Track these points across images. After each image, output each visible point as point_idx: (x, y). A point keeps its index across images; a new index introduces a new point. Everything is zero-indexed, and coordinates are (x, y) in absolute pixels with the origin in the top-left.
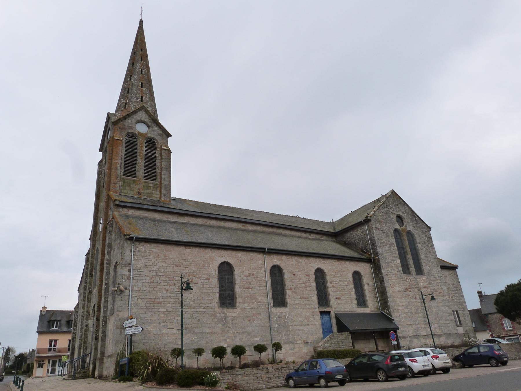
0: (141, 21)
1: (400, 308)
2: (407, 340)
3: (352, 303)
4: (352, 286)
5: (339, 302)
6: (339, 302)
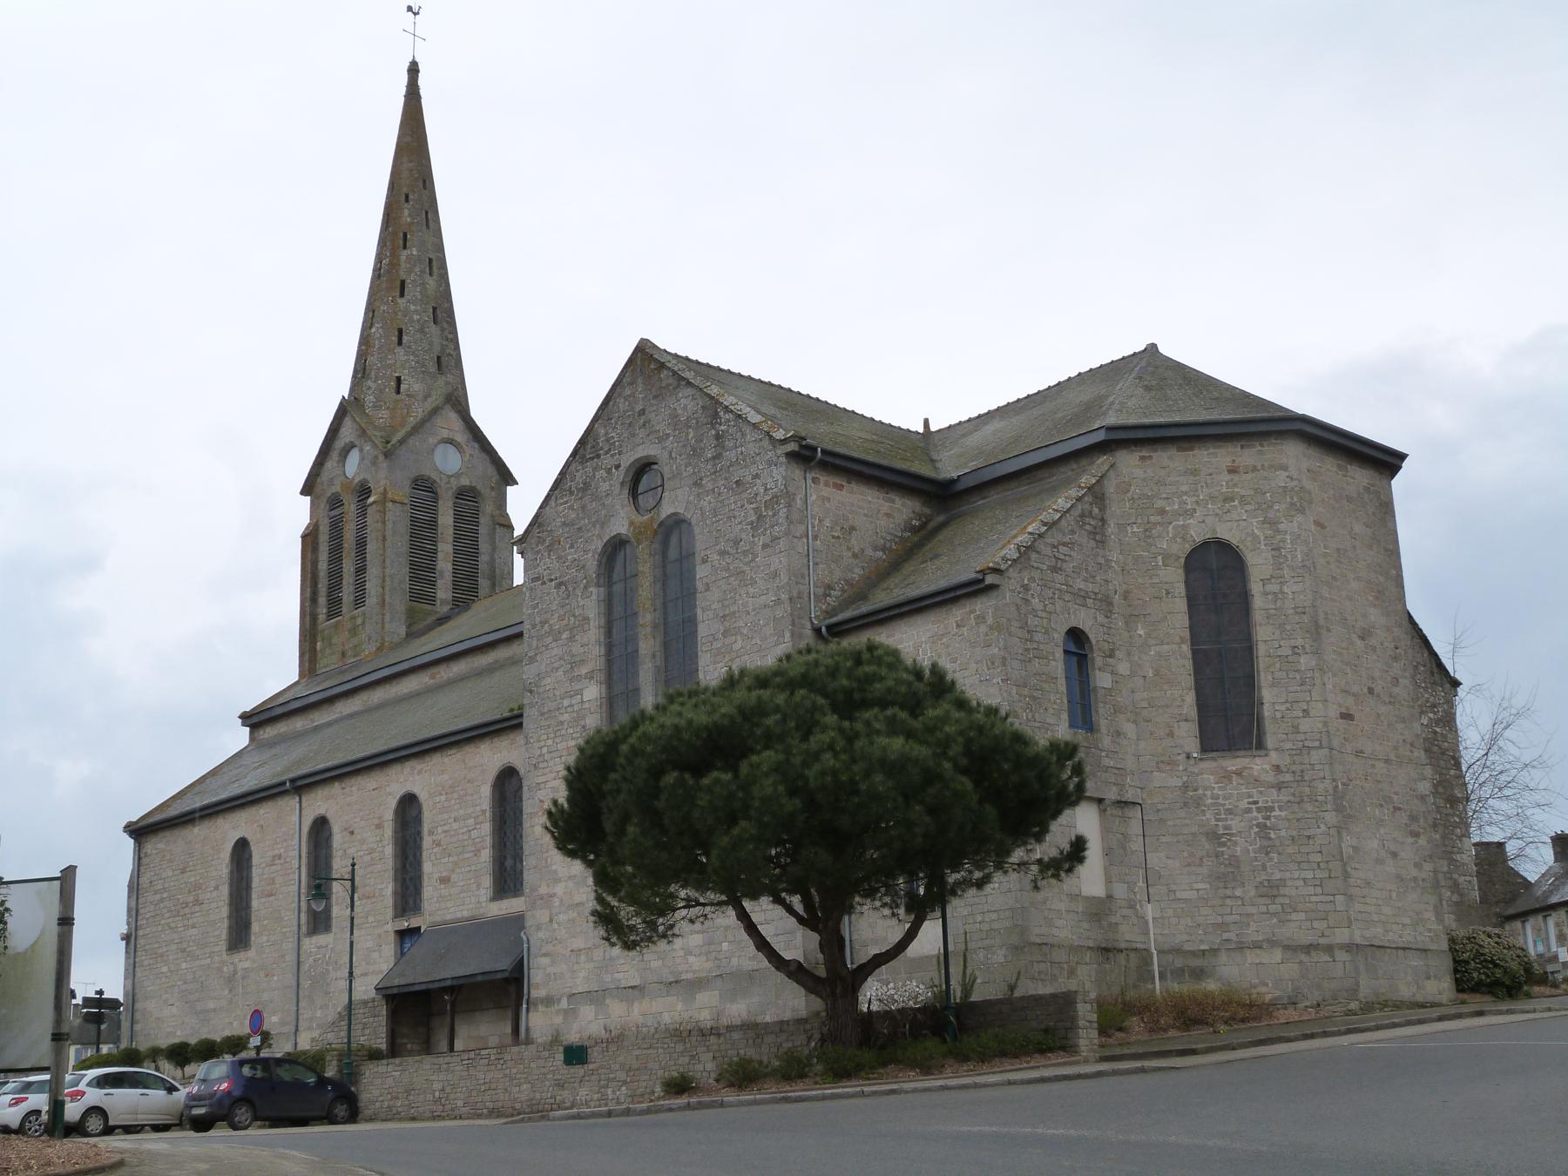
0: (414, 70)
1: (559, 889)
2: (558, 1012)
3: (478, 886)
4: (486, 829)
5: (445, 892)
6: (445, 892)
